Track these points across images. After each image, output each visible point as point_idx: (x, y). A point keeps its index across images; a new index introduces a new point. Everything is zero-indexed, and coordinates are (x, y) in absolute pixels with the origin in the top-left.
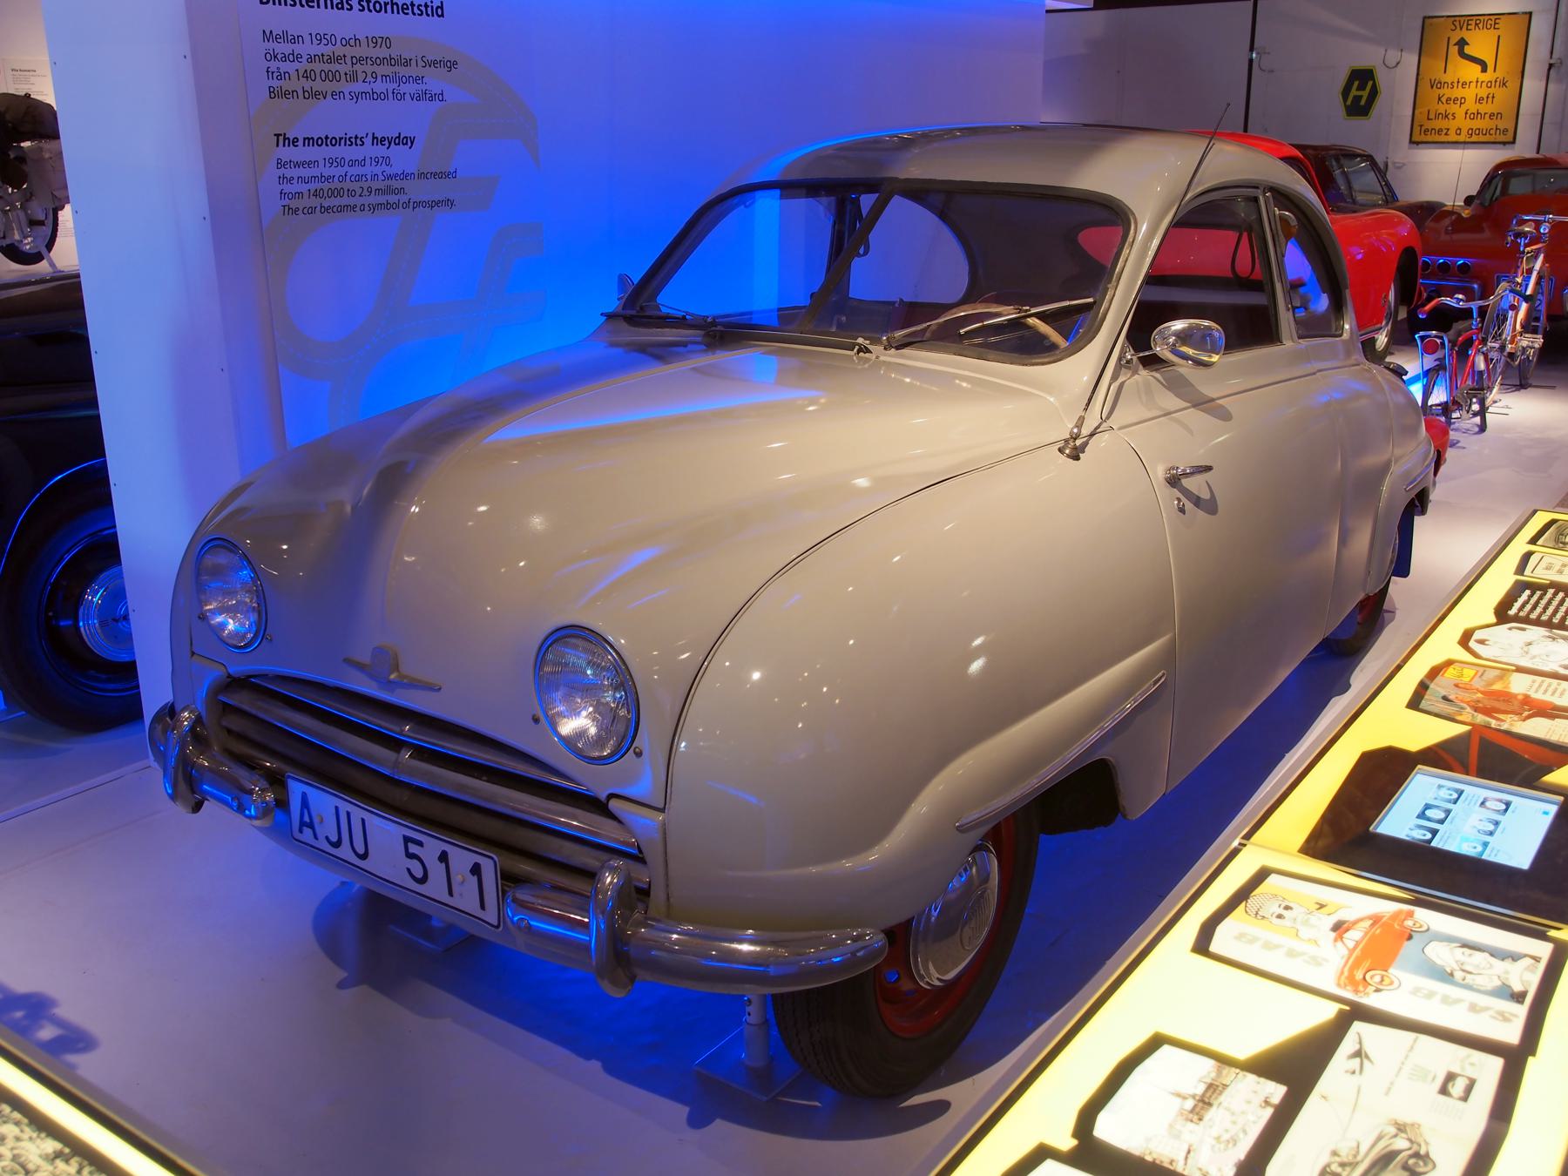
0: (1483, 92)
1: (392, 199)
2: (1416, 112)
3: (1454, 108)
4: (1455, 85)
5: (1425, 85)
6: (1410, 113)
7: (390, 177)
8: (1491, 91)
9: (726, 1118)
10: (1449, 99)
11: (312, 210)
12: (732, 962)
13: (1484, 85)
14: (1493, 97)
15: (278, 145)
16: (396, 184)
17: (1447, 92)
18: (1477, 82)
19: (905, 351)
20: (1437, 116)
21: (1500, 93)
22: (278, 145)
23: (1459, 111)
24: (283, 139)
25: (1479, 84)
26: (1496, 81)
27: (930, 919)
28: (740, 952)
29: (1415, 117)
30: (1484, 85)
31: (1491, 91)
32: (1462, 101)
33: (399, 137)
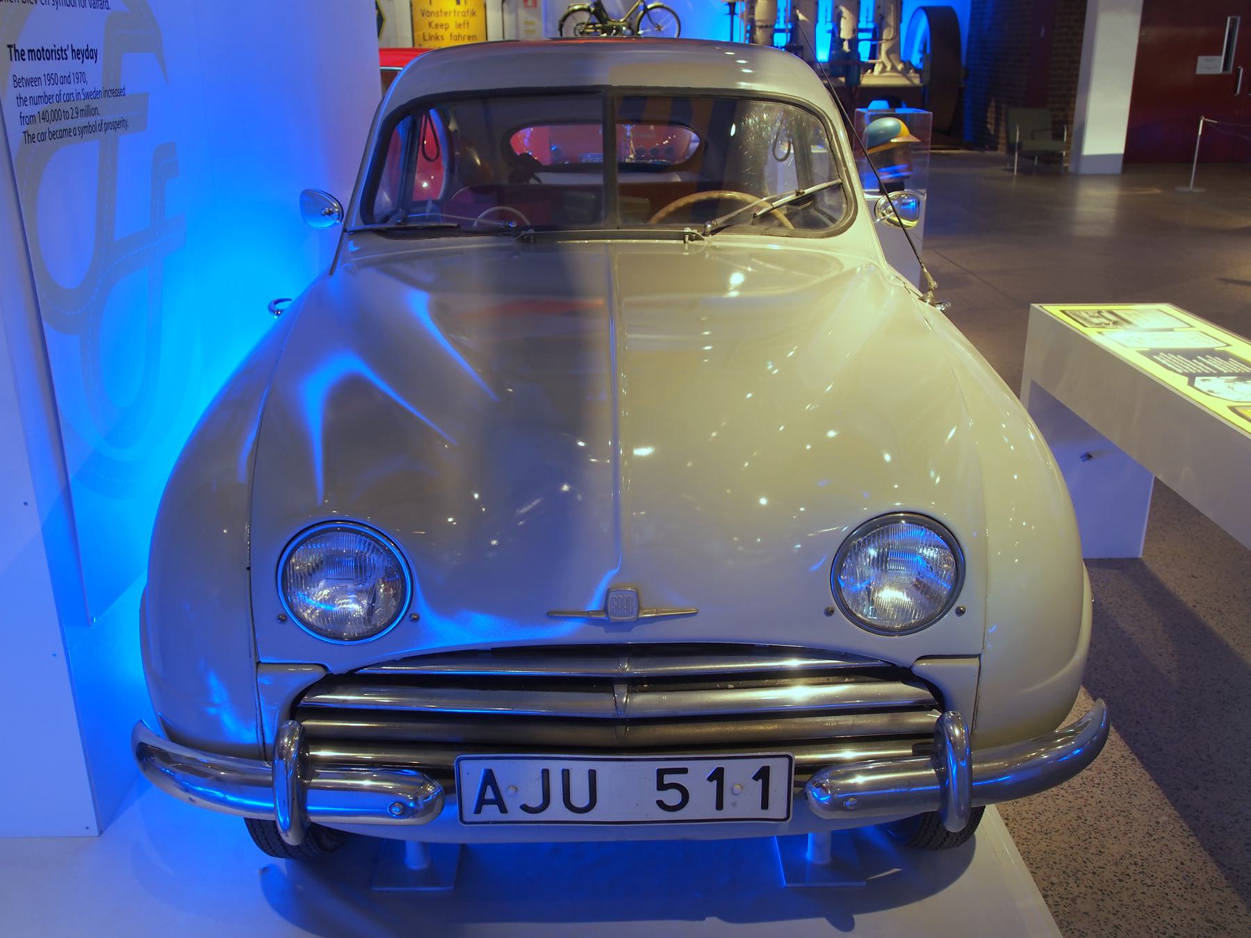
0: (461, 20)
1: (92, 120)
2: (415, 34)
3: (441, 32)
4: (440, 14)
5: (418, 15)
6: (410, 35)
7: (88, 96)
8: (466, 18)
9: (827, 918)
10: (437, 25)
11: (43, 137)
12: (855, 792)
13: (460, 14)
14: (468, 23)
15: (11, 60)
16: (93, 103)
17: (435, 20)
18: (455, 12)
19: (718, 236)
20: (431, 38)
21: (472, 20)
22: (11, 60)
23: (446, 35)
24: (17, 54)
25: (456, 14)
26: (468, 12)
27: (301, 700)
28: (855, 785)
29: (415, 39)
30: (460, 14)
31: (466, 18)
32: (446, 27)
33: (87, 50)
